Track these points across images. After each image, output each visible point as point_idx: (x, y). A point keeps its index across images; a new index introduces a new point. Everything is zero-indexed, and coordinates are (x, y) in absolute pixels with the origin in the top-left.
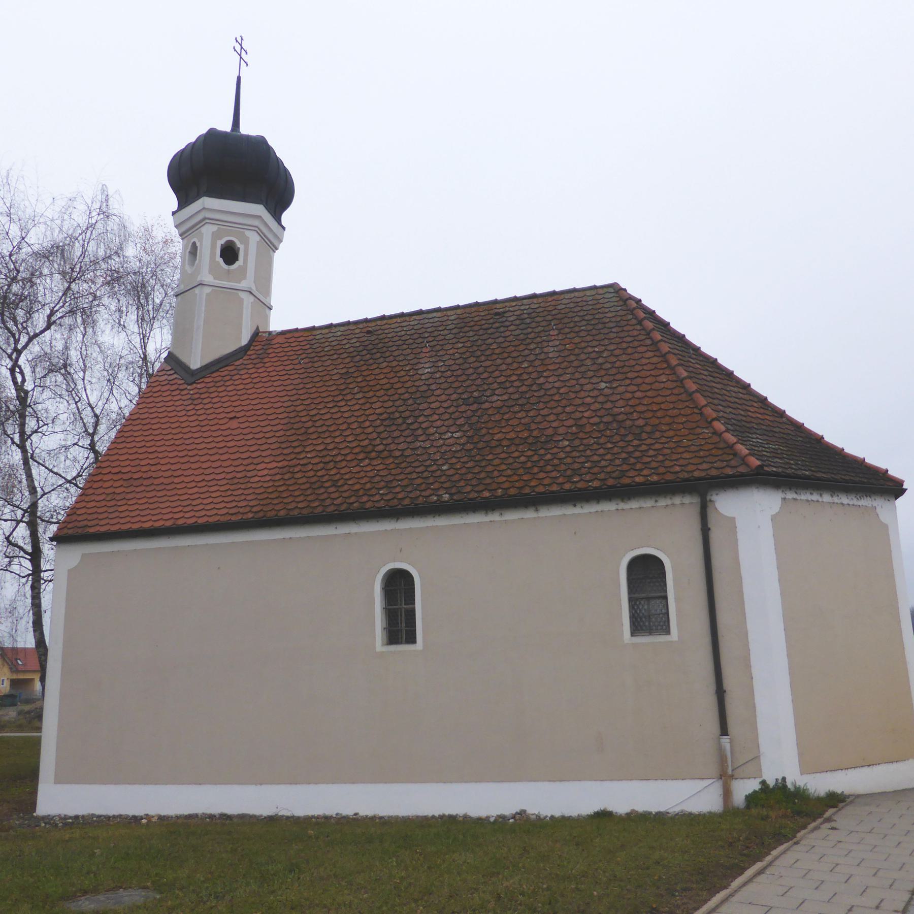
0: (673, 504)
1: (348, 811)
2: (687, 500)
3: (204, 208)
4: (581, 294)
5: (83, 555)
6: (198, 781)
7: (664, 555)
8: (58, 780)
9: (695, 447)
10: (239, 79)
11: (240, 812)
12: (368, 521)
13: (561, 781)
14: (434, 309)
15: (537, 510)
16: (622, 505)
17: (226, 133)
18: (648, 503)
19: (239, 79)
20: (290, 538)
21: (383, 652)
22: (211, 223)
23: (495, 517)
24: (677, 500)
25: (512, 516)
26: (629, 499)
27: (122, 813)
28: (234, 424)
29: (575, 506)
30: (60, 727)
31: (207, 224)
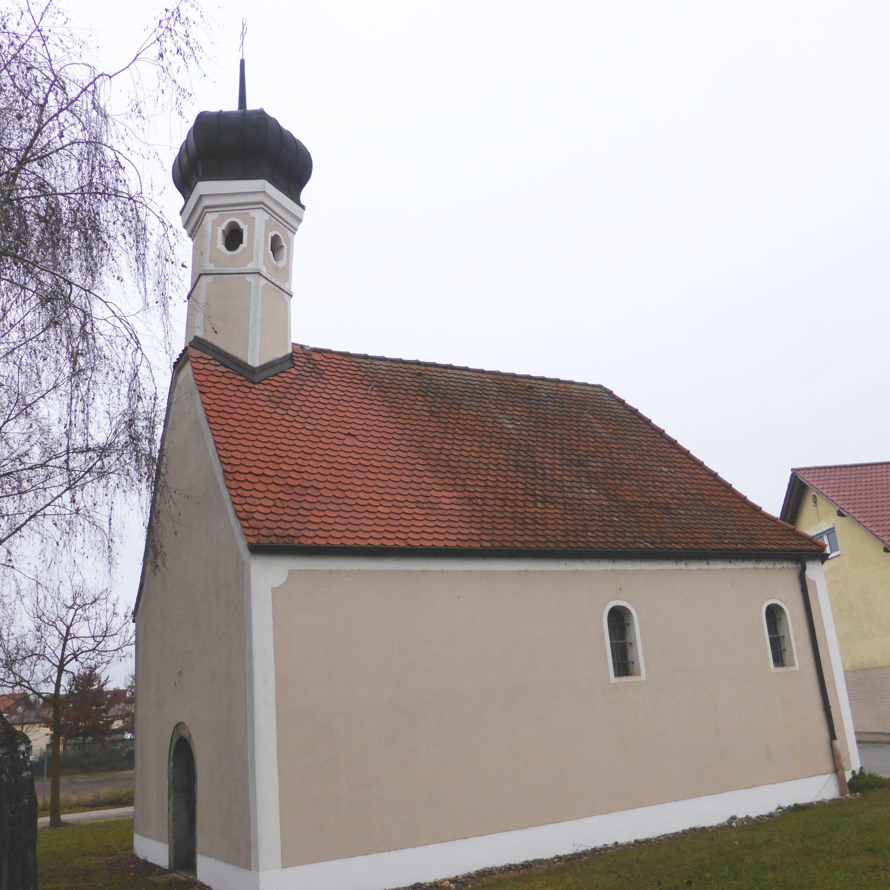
0: (783, 567)
1: (598, 842)
2: (791, 565)
3: (264, 192)
4: (576, 387)
5: (290, 572)
6: (593, 811)
7: (636, 614)
8: (287, 862)
9: (281, 531)
10: (242, 63)
11: (479, 867)
12: (591, 561)
13: (465, 838)
14: (489, 371)
15: (708, 563)
16: (757, 565)
17: (236, 111)
18: (749, 565)
19: (242, 63)
20: (526, 571)
21: (617, 683)
22: (266, 211)
23: (681, 566)
24: (785, 565)
25: (693, 566)
26: (760, 561)
27: (423, 882)
28: (349, 441)
29: (730, 562)
30: (284, 793)
31: (261, 210)
